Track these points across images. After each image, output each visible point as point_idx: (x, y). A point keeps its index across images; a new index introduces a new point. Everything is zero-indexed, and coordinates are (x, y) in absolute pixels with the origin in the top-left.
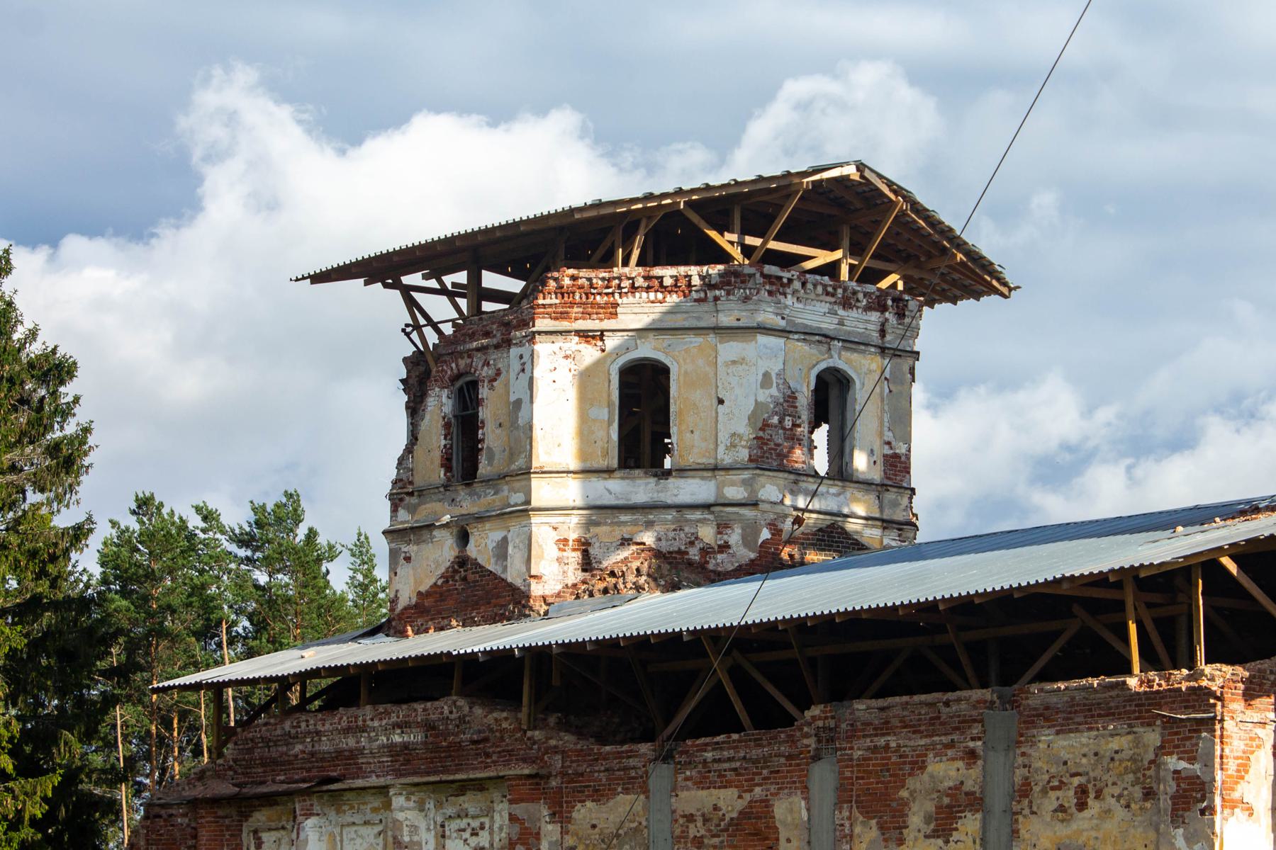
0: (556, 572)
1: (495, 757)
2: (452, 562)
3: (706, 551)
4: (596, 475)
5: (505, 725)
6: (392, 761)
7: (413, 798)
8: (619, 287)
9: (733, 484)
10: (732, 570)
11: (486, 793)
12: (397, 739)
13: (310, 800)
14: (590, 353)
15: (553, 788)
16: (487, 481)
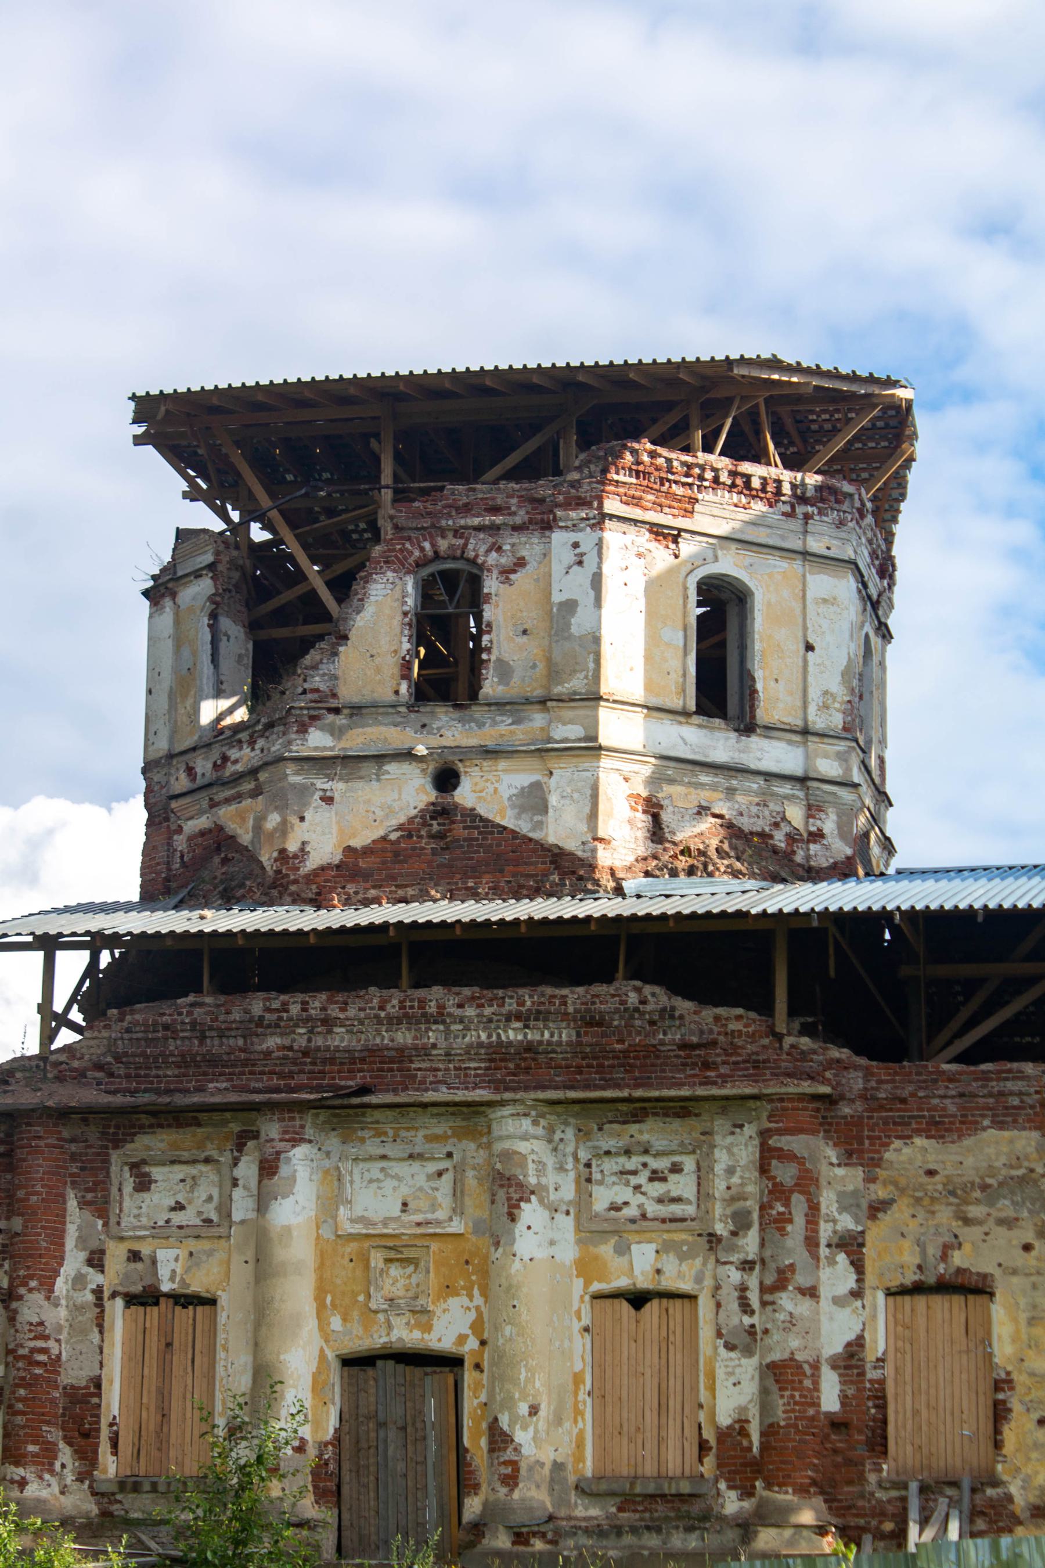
0: (628, 838)
1: (723, 1070)
2: (422, 811)
3: (792, 838)
4: (671, 716)
5: (733, 1026)
6: (487, 1069)
7: (543, 1122)
8: (701, 478)
9: (826, 756)
10: (827, 868)
11: (692, 1121)
12: (513, 1034)
13: (301, 1118)
14: (661, 557)
15: (845, 1117)
16: (500, 705)
